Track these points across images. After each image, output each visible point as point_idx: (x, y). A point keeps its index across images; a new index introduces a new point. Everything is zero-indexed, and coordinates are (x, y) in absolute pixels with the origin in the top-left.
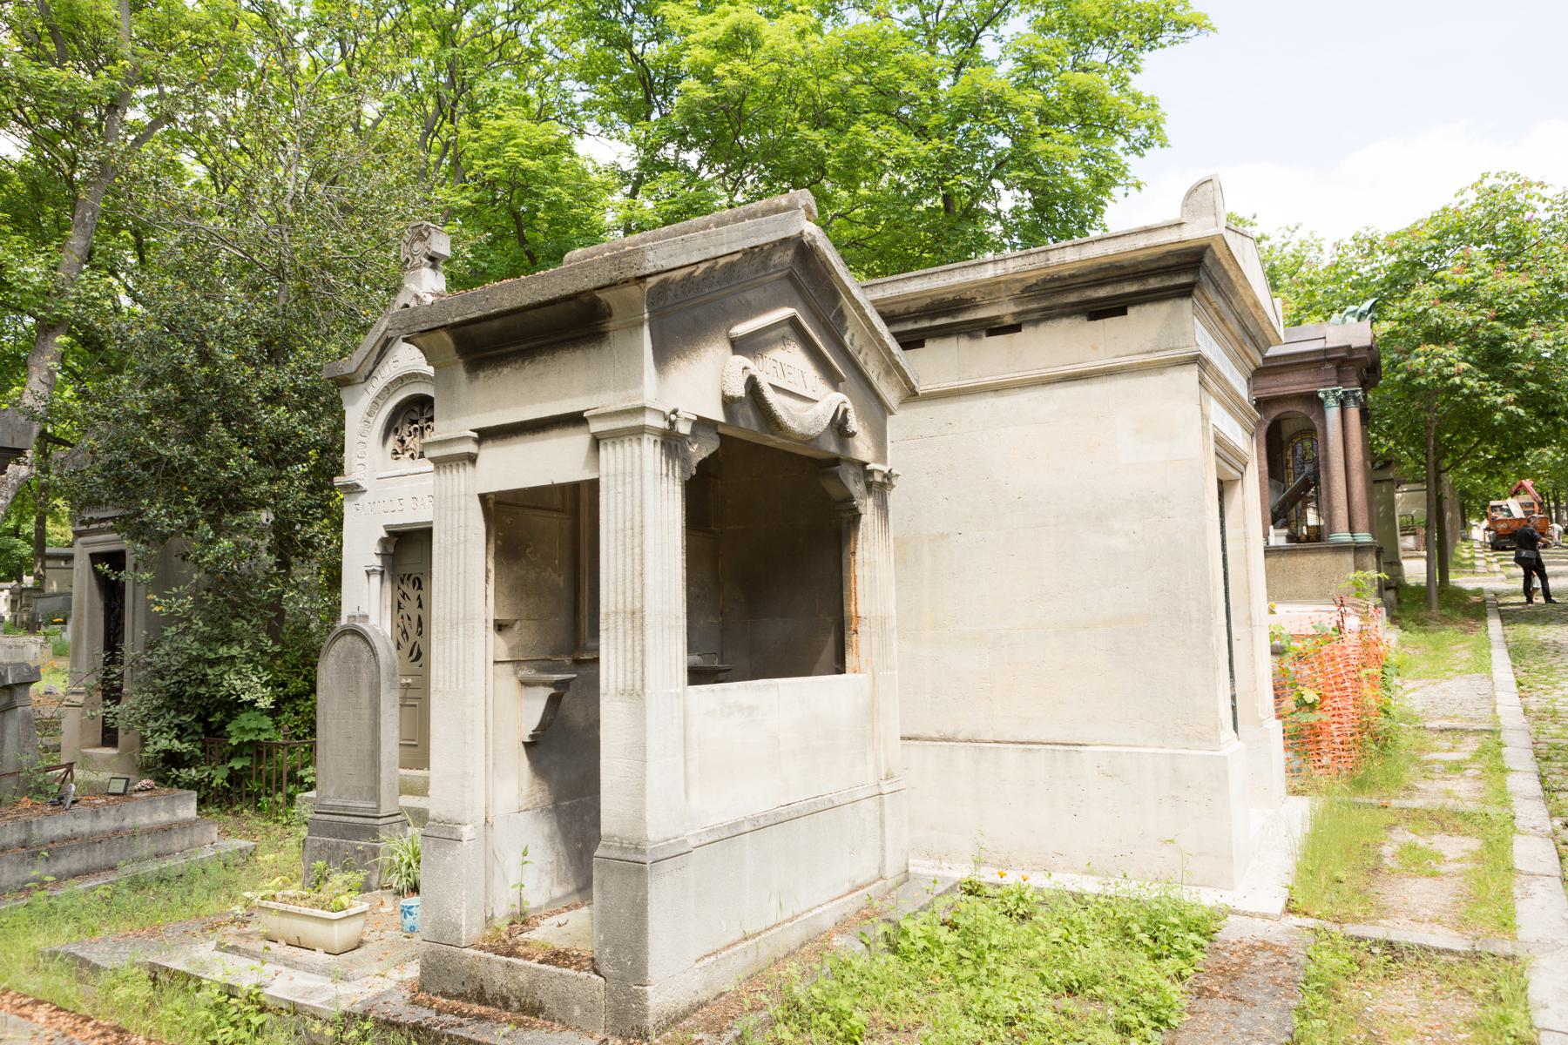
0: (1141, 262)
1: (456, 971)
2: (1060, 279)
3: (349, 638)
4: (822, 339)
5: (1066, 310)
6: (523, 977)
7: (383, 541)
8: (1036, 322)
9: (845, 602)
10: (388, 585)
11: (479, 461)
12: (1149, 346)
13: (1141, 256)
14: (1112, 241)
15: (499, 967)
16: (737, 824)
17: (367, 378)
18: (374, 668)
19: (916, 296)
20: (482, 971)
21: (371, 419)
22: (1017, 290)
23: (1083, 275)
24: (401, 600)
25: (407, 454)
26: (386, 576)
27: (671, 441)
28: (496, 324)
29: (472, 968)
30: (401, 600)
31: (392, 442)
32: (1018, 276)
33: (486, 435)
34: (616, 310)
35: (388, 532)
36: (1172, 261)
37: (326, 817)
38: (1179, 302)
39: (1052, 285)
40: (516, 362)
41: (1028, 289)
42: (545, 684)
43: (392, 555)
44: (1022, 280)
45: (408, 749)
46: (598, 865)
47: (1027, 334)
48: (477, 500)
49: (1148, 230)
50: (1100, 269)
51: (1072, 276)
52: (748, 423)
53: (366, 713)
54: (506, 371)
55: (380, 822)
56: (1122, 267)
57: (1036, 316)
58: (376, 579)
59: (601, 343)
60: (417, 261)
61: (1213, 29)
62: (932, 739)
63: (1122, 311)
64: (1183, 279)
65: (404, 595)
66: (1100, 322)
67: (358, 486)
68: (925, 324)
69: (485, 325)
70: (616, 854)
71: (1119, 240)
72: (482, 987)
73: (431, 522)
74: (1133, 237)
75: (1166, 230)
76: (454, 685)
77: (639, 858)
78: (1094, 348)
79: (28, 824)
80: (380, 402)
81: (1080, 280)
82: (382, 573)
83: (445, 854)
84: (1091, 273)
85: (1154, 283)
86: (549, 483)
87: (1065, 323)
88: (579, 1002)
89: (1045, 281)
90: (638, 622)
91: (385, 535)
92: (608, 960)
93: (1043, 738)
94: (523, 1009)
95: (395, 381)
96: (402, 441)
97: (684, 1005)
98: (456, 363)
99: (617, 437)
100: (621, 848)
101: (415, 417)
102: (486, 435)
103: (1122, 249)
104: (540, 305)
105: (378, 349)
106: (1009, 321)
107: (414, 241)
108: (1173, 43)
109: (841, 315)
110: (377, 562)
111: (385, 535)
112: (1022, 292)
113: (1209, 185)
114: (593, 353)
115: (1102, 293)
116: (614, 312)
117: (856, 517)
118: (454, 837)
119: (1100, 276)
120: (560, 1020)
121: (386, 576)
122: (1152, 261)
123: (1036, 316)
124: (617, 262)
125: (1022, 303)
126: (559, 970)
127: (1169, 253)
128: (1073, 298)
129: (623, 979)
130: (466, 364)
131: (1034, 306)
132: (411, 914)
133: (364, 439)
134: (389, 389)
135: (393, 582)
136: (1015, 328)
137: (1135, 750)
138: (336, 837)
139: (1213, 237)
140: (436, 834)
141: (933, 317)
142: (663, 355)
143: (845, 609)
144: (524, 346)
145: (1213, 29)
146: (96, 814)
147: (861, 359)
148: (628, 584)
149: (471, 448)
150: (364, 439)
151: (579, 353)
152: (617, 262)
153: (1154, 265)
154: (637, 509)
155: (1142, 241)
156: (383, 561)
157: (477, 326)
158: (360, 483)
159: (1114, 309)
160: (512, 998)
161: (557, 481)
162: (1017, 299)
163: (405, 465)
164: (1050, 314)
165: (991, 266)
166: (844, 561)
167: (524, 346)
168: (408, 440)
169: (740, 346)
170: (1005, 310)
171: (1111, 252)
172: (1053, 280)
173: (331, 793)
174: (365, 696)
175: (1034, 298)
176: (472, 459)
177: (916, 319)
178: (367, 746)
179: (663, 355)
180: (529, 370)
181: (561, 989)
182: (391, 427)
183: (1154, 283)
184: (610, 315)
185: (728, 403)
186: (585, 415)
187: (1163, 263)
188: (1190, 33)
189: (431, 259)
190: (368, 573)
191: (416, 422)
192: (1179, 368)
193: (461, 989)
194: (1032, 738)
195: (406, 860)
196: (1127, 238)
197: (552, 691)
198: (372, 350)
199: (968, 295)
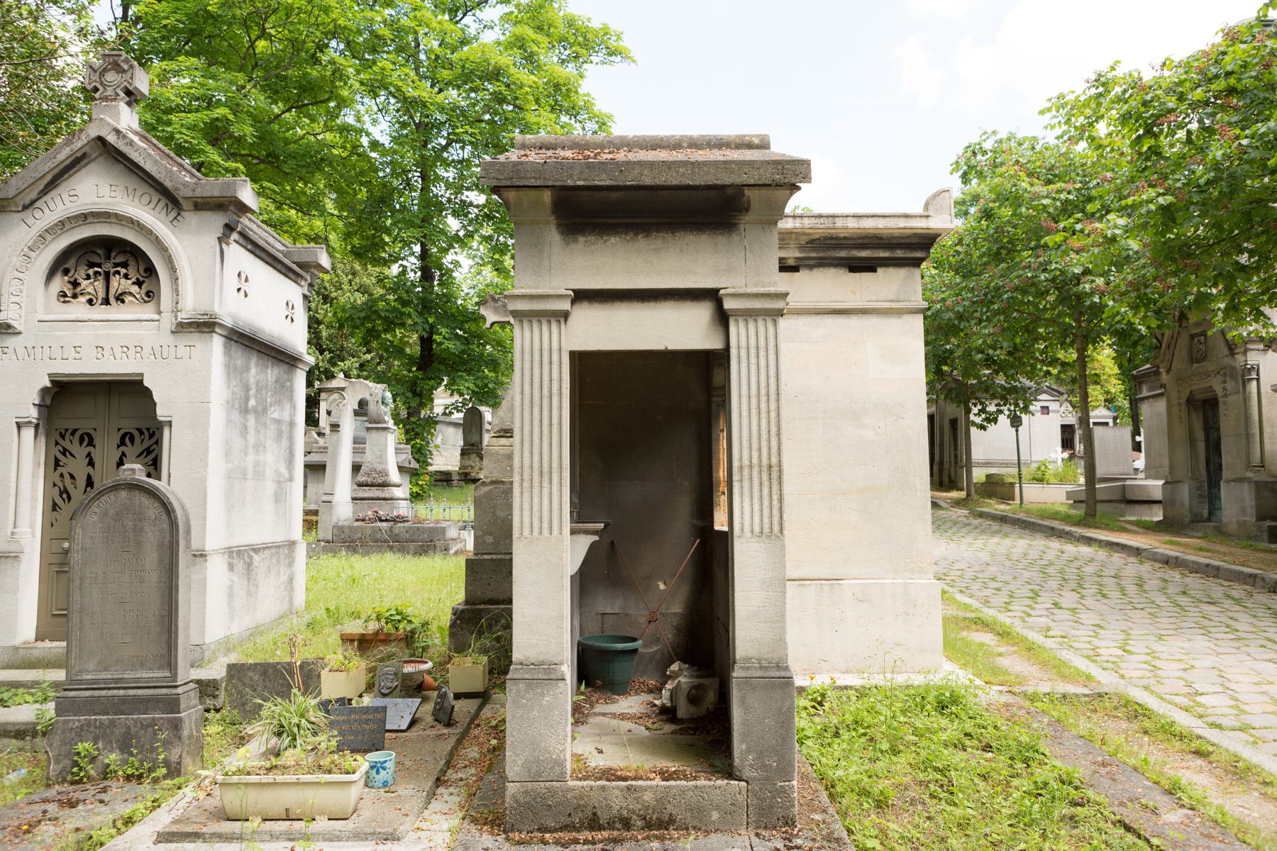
0: (895, 238)
1: (559, 804)
2: (836, 238)
3: (123, 494)
5: (834, 262)
6: (648, 797)
7: (44, 391)
8: (811, 267)
9: (714, 469)
10: (42, 440)
11: (570, 319)
12: (891, 297)
13: (896, 233)
14: (881, 219)
15: (617, 792)
17: (25, 208)
18: (166, 526)
20: (595, 798)
21: (32, 254)
22: (804, 240)
23: (854, 239)
24: (60, 457)
25: (83, 299)
26: (41, 430)
28: (615, 195)
29: (582, 798)
30: (60, 457)
31: (59, 283)
32: (807, 231)
33: (582, 296)
34: (755, 205)
35: (52, 382)
36: (915, 241)
37: (87, 693)
38: (912, 269)
39: (829, 242)
40: (626, 233)
41: (812, 241)
42: (587, 532)
43: (47, 407)
44: (810, 234)
45: (58, 620)
46: (739, 685)
49: (906, 216)
50: (867, 237)
51: (845, 238)
53: (153, 577)
54: (613, 240)
55: (180, 690)
56: (881, 238)
57: (812, 262)
58: (29, 433)
59: (730, 232)
60: (110, 92)
61: (634, 61)
64: (919, 254)
65: (65, 452)
66: (857, 275)
67: (9, 326)
69: (604, 194)
70: (759, 673)
71: (887, 219)
72: (595, 814)
73: (142, 375)
74: (896, 219)
75: (918, 219)
76: (546, 531)
77: (783, 674)
78: (854, 293)
80: (49, 238)
81: (851, 242)
82: (37, 427)
83: (543, 694)
84: (859, 238)
85: (899, 253)
86: (662, 348)
87: (833, 271)
88: (718, 808)
89: (826, 238)
90: (775, 475)
91: (49, 385)
92: (751, 766)
93: (810, 576)
94: (649, 825)
95: (76, 217)
96: (75, 284)
98: (547, 223)
99: (751, 316)
100: (761, 668)
101: (96, 259)
102: (582, 296)
103: (889, 226)
104: (688, 187)
105: (49, 178)
107: (105, 70)
108: (603, 63)
110: (33, 413)
111: (49, 385)
112: (807, 243)
113: (947, 194)
114: (721, 240)
115: (864, 254)
116: (752, 208)
118: (553, 676)
119: (865, 242)
120: (694, 828)
121: (41, 430)
122: (902, 238)
123: (812, 262)
124: (780, 167)
125: (805, 251)
126: (693, 783)
127: (915, 235)
128: (843, 254)
129: (767, 779)
130: (559, 226)
131: (814, 255)
132: (384, 769)
133: (20, 275)
134: (63, 225)
135: (48, 436)
137: (878, 581)
138: (107, 714)
139: (945, 230)
140: (527, 676)
143: (714, 475)
144: (638, 221)
145: (634, 61)
148: (764, 443)
149: (565, 305)
150: (20, 275)
151: (704, 237)
152: (780, 167)
153: (903, 241)
154: (772, 380)
155: (902, 223)
156: (40, 413)
157: (591, 193)
158: (10, 321)
159: (868, 266)
160: (635, 817)
161: (672, 347)
162: (801, 248)
163: (78, 308)
164: (822, 263)
165: (790, 220)
166: (714, 437)
167: (638, 221)
168: (84, 283)
171: (881, 226)
172: (831, 238)
173: (91, 666)
174: (151, 557)
175: (813, 249)
176: (565, 315)
178: (154, 607)
180: (642, 243)
181: (694, 800)
182: (60, 266)
183: (899, 253)
184: (747, 210)
186: (722, 292)
187: (908, 241)
188: (618, 59)
189: (128, 93)
190: (19, 426)
191: (99, 266)
192: (912, 315)
193: (568, 821)
194: (802, 576)
196: (892, 219)
197: (597, 538)
198: (41, 178)
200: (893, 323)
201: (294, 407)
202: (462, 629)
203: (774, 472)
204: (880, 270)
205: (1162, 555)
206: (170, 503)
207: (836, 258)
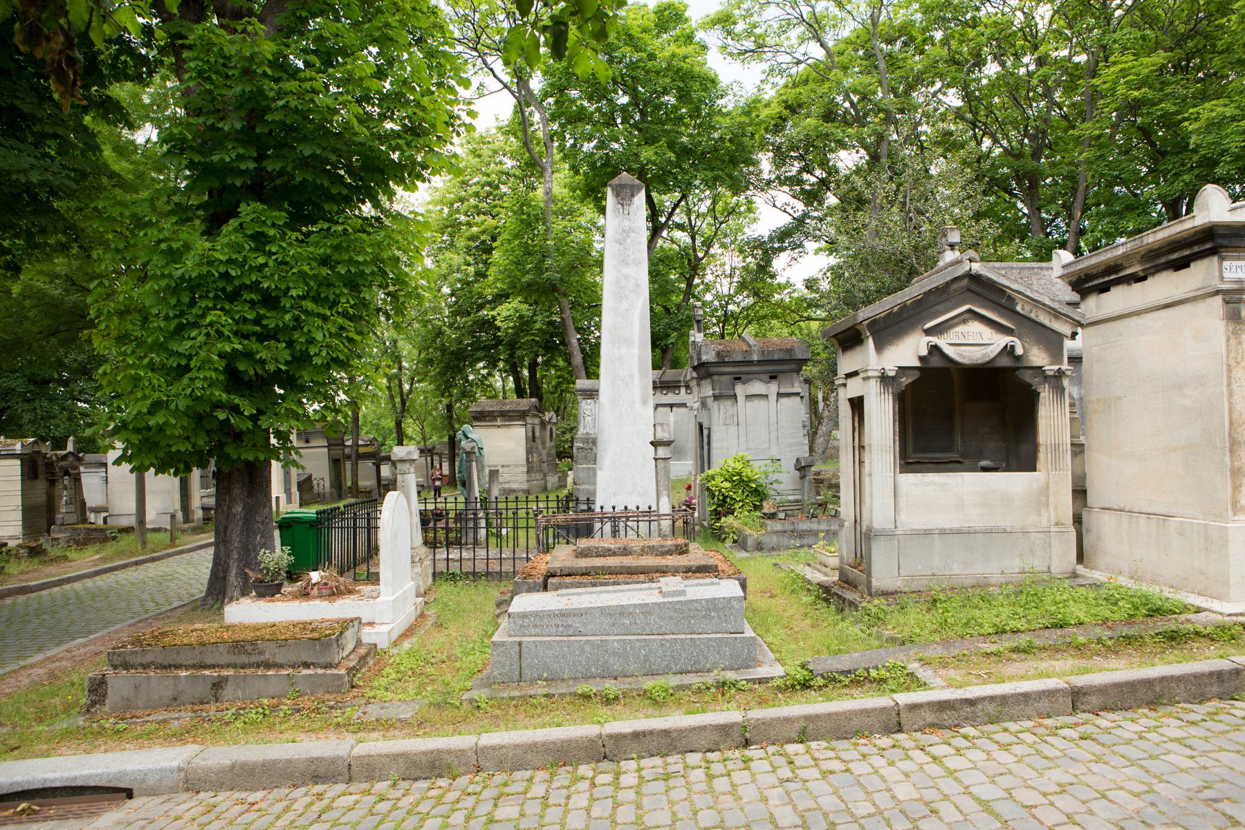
2: (1154, 250)
4: (1001, 316)
8: (1153, 274)
16: (930, 530)
19: (1099, 264)
27: (884, 379)
47: (1150, 282)
48: (848, 403)
50: (1169, 244)
51: (1159, 248)
52: (936, 362)
56: (1179, 242)
57: (1152, 270)
62: (1116, 510)
63: (1188, 266)
68: (1106, 279)
79: (793, 523)
85: (1196, 249)
97: (893, 590)
106: (1142, 274)
109: (1011, 299)
115: (1174, 256)
117: (1036, 395)
128: (1163, 260)
136: (1144, 278)
141: (1109, 275)
142: (879, 348)
146: (819, 522)
147: (1033, 316)
149: (844, 381)
162: (1140, 262)
169: (928, 332)
170: (1136, 269)
172: (1151, 251)
175: (1148, 261)
177: (1103, 276)
179: (879, 348)
183: (1196, 249)
185: (921, 359)
187: (1196, 238)
195: (747, 513)
199: (1119, 262)
200: (1201, 306)
201: (420, 725)
202: (433, 126)
203: (870, 475)
204: (1192, 265)
205: (39, 290)
206: (81, 795)
207: (1162, 264)
